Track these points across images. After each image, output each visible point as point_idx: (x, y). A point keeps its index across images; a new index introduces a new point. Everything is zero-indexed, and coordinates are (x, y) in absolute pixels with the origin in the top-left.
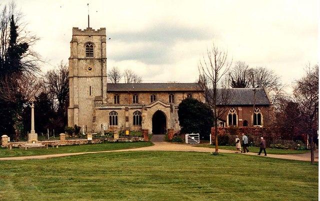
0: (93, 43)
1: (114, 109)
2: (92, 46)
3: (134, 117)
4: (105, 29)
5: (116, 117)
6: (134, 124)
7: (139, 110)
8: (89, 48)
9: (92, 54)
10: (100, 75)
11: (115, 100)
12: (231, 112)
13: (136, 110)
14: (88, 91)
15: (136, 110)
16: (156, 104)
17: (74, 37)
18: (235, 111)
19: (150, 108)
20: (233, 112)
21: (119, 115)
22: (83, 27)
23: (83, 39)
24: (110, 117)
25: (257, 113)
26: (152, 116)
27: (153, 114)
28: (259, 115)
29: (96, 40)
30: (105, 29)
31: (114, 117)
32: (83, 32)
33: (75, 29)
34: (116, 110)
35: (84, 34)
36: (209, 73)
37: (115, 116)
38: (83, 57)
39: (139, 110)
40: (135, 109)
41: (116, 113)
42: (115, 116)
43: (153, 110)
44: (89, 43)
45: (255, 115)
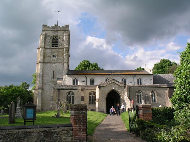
0: (57, 36)
2: (57, 39)
3: (90, 97)
5: (73, 97)
6: (90, 103)
8: (55, 42)
10: (46, 61)
11: (90, 101)
13: (69, 91)
14: (51, 75)
15: (91, 91)
17: (62, 78)
21: (75, 95)
23: (51, 33)
24: (67, 97)
26: (105, 96)
29: (60, 34)
31: (70, 97)
34: (72, 90)
37: (72, 96)
38: (48, 47)
41: (72, 93)
42: (72, 96)
43: (107, 90)
44: (55, 36)
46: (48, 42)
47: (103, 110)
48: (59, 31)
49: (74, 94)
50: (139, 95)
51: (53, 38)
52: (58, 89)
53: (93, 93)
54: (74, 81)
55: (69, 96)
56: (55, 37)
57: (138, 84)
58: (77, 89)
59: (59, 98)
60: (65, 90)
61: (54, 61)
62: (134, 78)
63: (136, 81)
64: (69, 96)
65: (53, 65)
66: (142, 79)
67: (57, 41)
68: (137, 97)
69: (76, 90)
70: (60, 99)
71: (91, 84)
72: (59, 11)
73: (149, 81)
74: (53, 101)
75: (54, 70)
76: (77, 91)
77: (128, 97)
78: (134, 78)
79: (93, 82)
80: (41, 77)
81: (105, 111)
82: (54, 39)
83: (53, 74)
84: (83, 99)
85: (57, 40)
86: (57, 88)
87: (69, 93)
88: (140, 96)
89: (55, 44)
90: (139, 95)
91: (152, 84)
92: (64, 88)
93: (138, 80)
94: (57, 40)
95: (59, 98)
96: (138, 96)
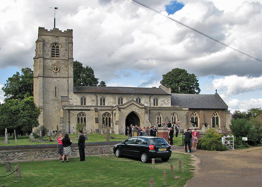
1: (107, 110)
3: (104, 118)
4: (72, 30)
5: (85, 118)
7: (108, 112)
9: (58, 55)
10: (45, 76)
12: (214, 115)
13: (80, 112)
16: (130, 105)
17: (67, 96)
18: (197, 114)
19: (123, 108)
20: (195, 115)
22: (49, 28)
23: (50, 40)
25: (215, 117)
27: (127, 115)
28: (217, 118)
29: (62, 40)
30: (72, 30)
31: (82, 118)
32: (63, 33)
33: (41, 30)
34: (83, 111)
35: (51, 34)
36: (247, 79)
39: (108, 112)
40: (104, 110)
41: (84, 114)
42: (83, 117)
43: (126, 112)
44: (56, 44)
45: (213, 118)
46: (47, 51)
47: (122, 133)
48: (60, 38)
49: (85, 116)
50: (159, 117)
51: (53, 46)
52: (68, 110)
53: (107, 114)
54: (82, 99)
55: (80, 118)
56: (56, 45)
57: (154, 105)
58: (89, 110)
59: (69, 120)
60: (75, 111)
61: (56, 76)
62: (150, 98)
63: (152, 101)
64: (80, 118)
65: (55, 80)
66: (141, 99)
67: (59, 50)
68: (157, 119)
69: (88, 112)
70: (71, 121)
71: (101, 104)
72: (56, 8)
73: (166, 101)
74: (63, 124)
75: (57, 86)
76: (90, 111)
77: (148, 119)
78: (150, 98)
79: (104, 101)
80: (42, 95)
81: (125, 134)
82: (53, 46)
83: (54, 91)
84: (98, 120)
85: (58, 49)
86: (66, 108)
87: (104, 114)
88: (160, 118)
89: (55, 53)
90: (159, 117)
91: (169, 105)
92: (75, 108)
93: (154, 100)
94: (58, 49)
95: (69, 120)
96: (158, 118)
